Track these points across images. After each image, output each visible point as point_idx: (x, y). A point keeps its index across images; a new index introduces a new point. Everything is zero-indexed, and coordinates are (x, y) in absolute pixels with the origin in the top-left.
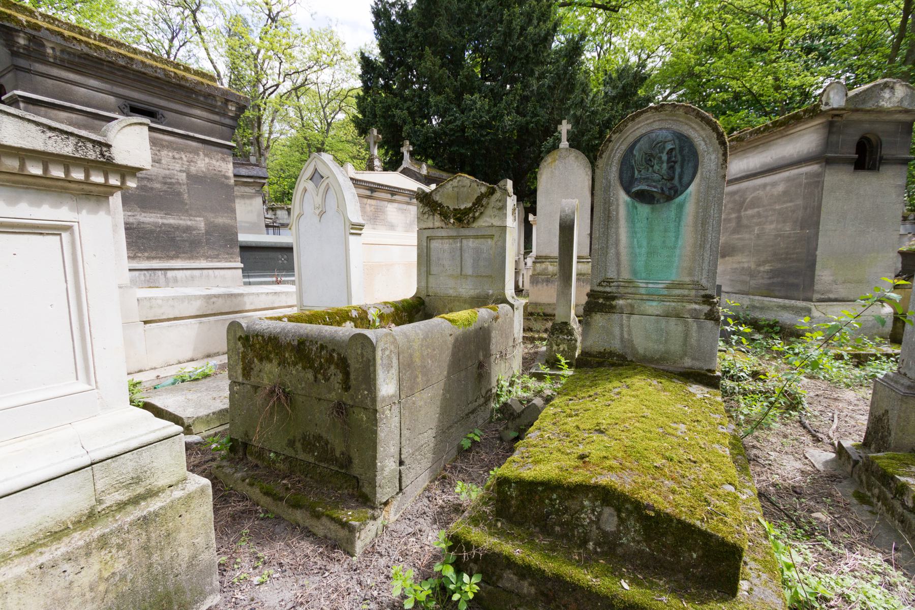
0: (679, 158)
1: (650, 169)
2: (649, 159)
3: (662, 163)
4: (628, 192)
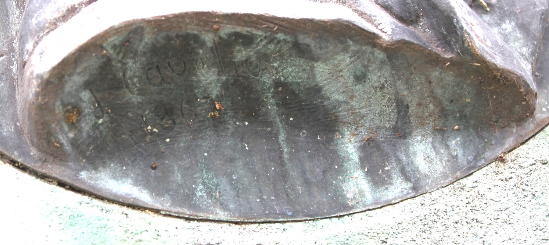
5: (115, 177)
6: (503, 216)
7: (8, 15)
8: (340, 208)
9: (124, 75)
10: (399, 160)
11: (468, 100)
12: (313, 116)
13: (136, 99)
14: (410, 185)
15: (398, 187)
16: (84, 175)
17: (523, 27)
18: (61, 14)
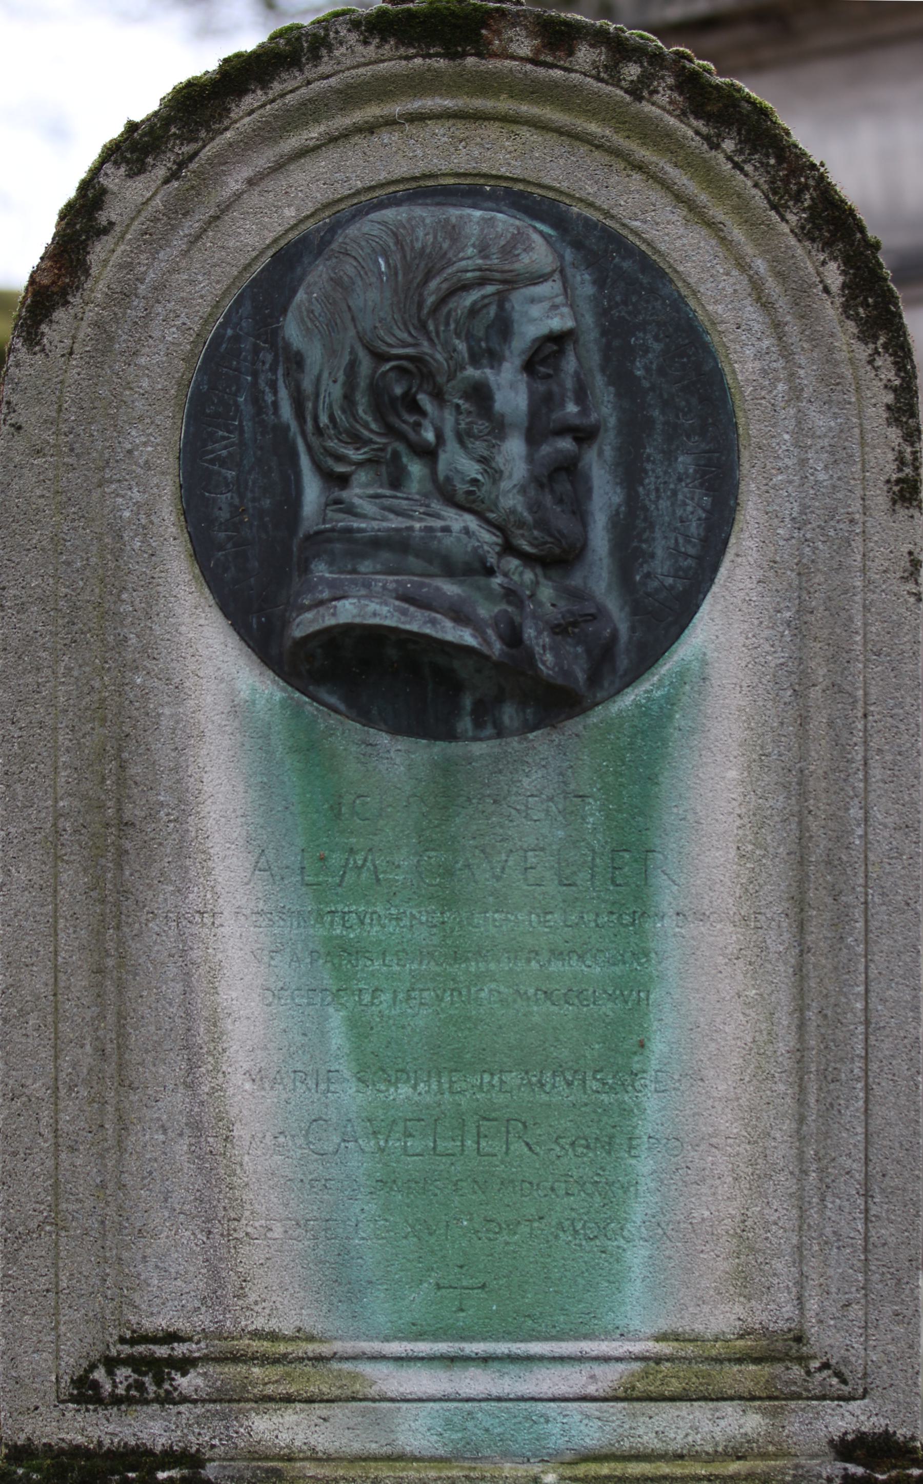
0: (606, 408)
2: (399, 399)
4: (257, 622)
6: (543, 763)
8: (451, 736)
12: (452, 686)
15: (489, 731)
17: (588, 652)
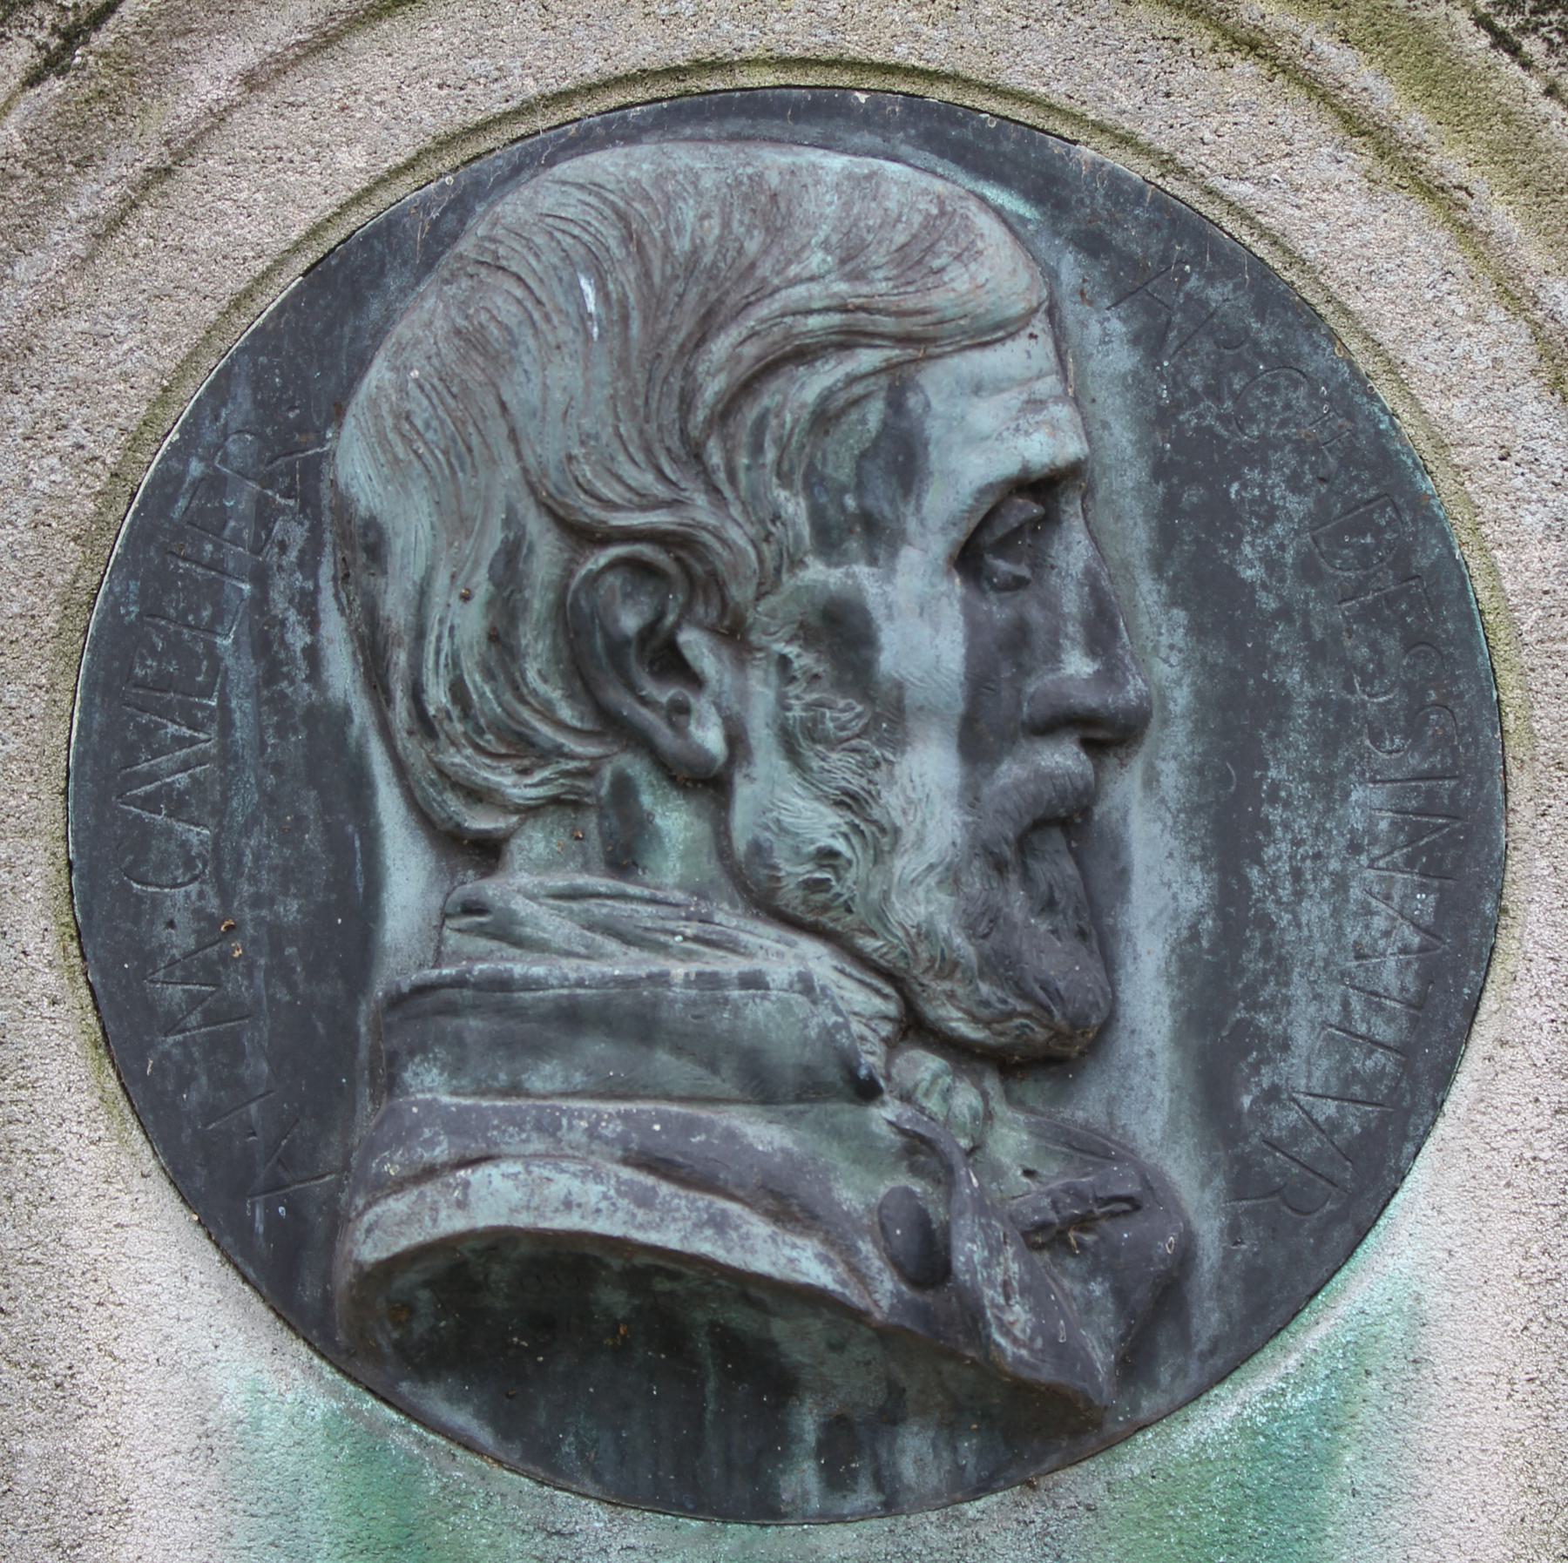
0: (1165, 665)
1: (675, 822)
2: (628, 640)
3: (890, 718)
4: (262, 1201)
5: (449, 1399)
7: (354, 1111)
9: (486, 1276)
10: (875, 1456)
11: (997, 1401)
13: (500, 1304)
14: (881, 1498)
15: (865, 1496)
16: (405, 1387)
17: (1120, 1294)
18: (412, 1173)
